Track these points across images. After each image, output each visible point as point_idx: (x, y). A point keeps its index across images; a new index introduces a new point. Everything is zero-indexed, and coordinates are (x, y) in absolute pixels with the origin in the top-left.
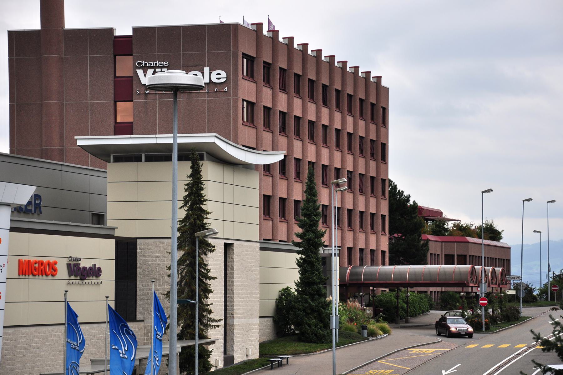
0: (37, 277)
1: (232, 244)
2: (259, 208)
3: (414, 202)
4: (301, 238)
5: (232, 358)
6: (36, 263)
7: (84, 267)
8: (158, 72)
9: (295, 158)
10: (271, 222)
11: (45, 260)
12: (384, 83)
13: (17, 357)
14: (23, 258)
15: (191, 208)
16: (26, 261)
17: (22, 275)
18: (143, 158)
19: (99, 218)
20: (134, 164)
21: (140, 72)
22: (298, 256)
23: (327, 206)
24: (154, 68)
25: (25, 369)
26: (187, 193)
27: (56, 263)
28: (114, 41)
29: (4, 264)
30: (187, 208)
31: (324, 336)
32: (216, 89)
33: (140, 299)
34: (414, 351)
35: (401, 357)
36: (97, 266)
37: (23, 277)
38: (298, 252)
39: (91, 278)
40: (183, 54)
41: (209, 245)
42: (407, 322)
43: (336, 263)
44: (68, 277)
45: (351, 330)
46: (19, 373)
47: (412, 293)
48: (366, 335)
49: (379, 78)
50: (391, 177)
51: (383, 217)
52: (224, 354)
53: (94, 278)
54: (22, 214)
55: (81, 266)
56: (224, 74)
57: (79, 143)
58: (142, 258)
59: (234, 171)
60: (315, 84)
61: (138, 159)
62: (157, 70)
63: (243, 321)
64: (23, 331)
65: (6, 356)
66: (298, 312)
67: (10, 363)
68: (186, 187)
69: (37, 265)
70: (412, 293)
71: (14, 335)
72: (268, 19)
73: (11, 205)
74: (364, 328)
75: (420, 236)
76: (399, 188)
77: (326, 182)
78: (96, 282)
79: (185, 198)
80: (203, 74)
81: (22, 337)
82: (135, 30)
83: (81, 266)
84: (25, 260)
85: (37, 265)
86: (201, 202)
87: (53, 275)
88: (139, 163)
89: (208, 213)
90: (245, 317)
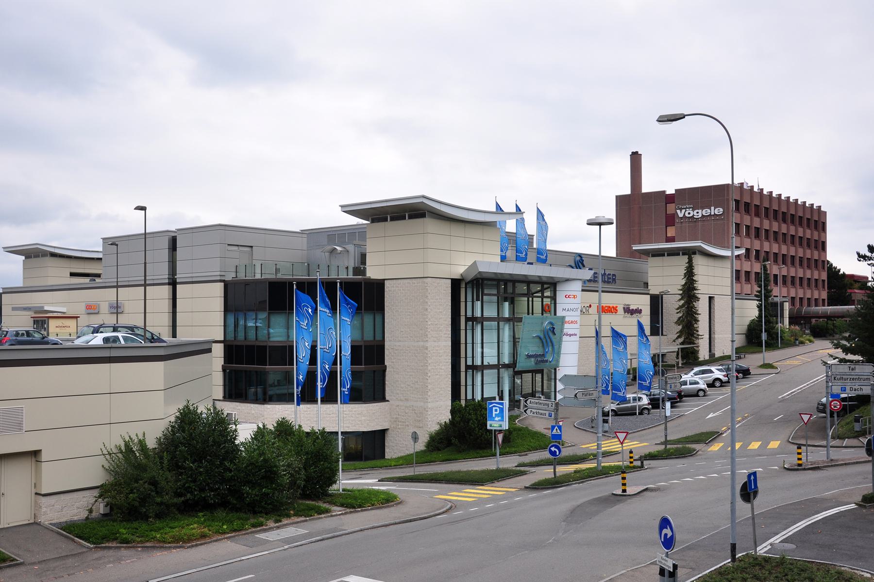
0: (607, 314)
1: (714, 297)
2: (119, 289)
3: (844, 272)
4: (759, 293)
5: (714, 354)
6: (606, 307)
7: (632, 309)
8: (25, 309)
9: (765, 251)
10: (750, 285)
11: (611, 305)
12: (822, 209)
15: (688, 278)
18: (666, 255)
19: (646, 285)
20: (661, 258)
21: (678, 211)
22: (757, 302)
23: (786, 276)
24: (686, 208)
26: (686, 271)
27: (617, 307)
28: (666, 197)
30: (685, 279)
31: (772, 344)
32: (718, 218)
33: (665, 325)
34: (821, 351)
35: (814, 354)
36: (639, 308)
38: (758, 300)
39: (637, 314)
40: (701, 201)
41: (697, 298)
42: (833, 337)
43: (787, 306)
45: (790, 341)
47: (838, 322)
48: (797, 343)
49: (820, 207)
50: (828, 259)
51: (823, 281)
52: (709, 352)
53: (638, 314)
54: (606, 284)
55: (631, 308)
56: (721, 210)
57: (634, 248)
58: (666, 304)
60: (778, 212)
61: (663, 255)
62: (687, 210)
63: (721, 336)
66: (757, 331)
68: (685, 268)
69: (607, 308)
70: (838, 322)
72: (682, 117)
74: (797, 340)
75: (846, 290)
76: (834, 265)
77: (786, 262)
78: (639, 316)
79: (685, 274)
80: (711, 210)
82: (676, 190)
83: (631, 308)
85: (607, 308)
86: (693, 276)
87: (616, 313)
88: (386, 223)
89: (697, 281)
90: (722, 334)
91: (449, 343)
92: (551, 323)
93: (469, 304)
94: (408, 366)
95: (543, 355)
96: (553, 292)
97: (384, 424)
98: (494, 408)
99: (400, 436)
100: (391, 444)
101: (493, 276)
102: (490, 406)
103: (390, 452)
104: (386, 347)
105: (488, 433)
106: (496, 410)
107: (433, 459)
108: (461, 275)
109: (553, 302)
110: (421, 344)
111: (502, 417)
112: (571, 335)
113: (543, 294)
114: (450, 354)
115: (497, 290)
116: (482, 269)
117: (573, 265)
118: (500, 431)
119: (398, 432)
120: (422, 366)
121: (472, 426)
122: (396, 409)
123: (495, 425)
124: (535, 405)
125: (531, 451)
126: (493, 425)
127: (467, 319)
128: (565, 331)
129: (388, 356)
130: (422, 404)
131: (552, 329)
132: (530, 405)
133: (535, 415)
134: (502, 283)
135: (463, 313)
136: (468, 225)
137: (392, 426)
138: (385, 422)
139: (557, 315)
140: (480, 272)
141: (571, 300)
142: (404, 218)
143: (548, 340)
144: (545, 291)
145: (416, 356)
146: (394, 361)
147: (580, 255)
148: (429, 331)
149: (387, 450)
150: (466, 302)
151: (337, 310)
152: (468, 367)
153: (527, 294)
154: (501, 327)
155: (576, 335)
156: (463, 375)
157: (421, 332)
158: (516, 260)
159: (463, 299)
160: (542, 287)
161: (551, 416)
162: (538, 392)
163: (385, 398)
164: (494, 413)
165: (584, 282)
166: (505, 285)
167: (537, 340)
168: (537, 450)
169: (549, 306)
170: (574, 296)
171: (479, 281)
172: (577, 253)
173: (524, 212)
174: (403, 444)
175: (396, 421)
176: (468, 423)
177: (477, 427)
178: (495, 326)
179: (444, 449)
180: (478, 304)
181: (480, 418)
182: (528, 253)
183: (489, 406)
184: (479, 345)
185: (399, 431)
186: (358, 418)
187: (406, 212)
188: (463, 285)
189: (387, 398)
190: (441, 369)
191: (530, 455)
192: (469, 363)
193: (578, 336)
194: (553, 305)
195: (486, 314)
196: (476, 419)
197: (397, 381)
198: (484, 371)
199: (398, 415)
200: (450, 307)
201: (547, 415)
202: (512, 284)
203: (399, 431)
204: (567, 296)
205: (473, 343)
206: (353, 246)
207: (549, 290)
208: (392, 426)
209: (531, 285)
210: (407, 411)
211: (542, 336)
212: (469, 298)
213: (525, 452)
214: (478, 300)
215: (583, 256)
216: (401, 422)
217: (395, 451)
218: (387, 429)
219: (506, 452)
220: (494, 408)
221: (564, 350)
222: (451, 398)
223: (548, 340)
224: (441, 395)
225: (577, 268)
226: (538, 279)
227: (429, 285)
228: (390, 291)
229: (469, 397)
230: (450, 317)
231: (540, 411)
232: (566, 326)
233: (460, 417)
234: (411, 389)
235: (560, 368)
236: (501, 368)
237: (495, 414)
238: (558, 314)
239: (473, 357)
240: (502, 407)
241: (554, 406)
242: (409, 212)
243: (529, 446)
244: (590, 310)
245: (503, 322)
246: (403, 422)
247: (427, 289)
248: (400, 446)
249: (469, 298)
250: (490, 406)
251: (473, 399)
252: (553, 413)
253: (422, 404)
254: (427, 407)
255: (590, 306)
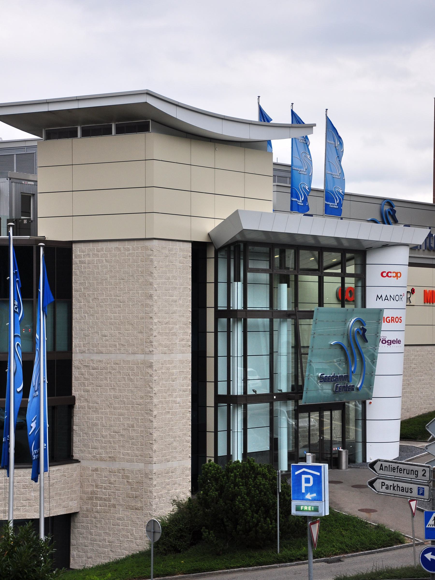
13: (424, 370)
14: (428, 289)
16: (431, 291)
17: (427, 303)
25: (432, 380)
29: (404, 294)
37: (428, 304)
44: (423, 304)
46: (426, 383)
54: (432, 252)
59: (215, 149)
64: (429, 349)
65: (415, 369)
67: (419, 375)
71: (421, 352)
73: (409, 245)
81: (428, 354)
84: (429, 291)
85: (390, 319)
88: (75, 140)
91: (189, 356)
92: (359, 321)
93: (222, 288)
94: (115, 397)
95: (347, 378)
96: (359, 267)
97: (71, 503)
98: (304, 477)
99: (99, 525)
100: (81, 541)
101: (262, 238)
102: (297, 473)
103: (79, 556)
104: (76, 362)
105: (268, 519)
106: (307, 481)
107: (169, 570)
108: (209, 234)
109: (360, 284)
110: (140, 357)
111: (319, 493)
112: (390, 342)
113: (343, 269)
114: (190, 376)
115: (268, 263)
116: (247, 225)
117: (378, 219)
118: (314, 520)
119: (95, 518)
120: (142, 398)
121: (241, 505)
122: (92, 475)
123: (306, 508)
124: (392, 473)
125: (347, 553)
126: (302, 508)
127: (219, 314)
128: (383, 335)
129: (77, 379)
130: (141, 466)
131: (361, 332)
132: (381, 472)
133: (391, 491)
134: (277, 250)
135: (210, 302)
136: (218, 146)
137: (85, 508)
138: (72, 500)
139: (368, 307)
140: (243, 232)
141: (392, 281)
142: (107, 132)
143: (355, 351)
144: (347, 263)
145: (131, 380)
146: (89, 388)
147: (390, 202)
148: (154, 334)
149: (74, 552)
150: (216, 283)
151: (8, 296)
152: (219, 399)
153: (318, 270)
154: (275, 328)
155: (399, 342)
156: (210, 412)
157: (140, 336)
158: (292, 209)
159: (210, 277)
160: (343, 256)
161: (423, 494)
162: (337, 443)
163: (73, 456)
164: (304, 485)
165: (414, 248)
166: (282, 253)
167: (338, 351)
168: (357, 551)
169: (351, 291)
170: (397, 273)
171: (239, 246)
172: (384, 199)
173: (315, 125)
174: (105, 540)
175: (91, 499)
176: (233, 500)
177: (250, 508)
178: (264, 326)
179: (186, 549)
180: (238, 287)
181: (255, 490)
182: (309, 198)
183: (294, 473)
184: (240, 361)
185: (98, 515)
186: (23, 494)
187: (111, 120)
188: (211, 253)
189: (76, 456)
190: (175, 402)
191: (346, 560)
192: (222, 390)
193: (403, 343)
194: (359, 290)
195: (251, 305)
196: (248, 494)
197: (95, 425)
198: (249, 406)
199: (97, 486)
200: (191, 293)
201: (415, 491)
202: (293, 251)
203: (98, 515)
204: (385, 274)
205: (229, 356)
206: (8, 182)
207: (353, 262)
208: (85, 508)
209: (325, 254)
210: (112, 479)
211: (345, 343)
212: (222, 276)
213: (336, 554)
214: (237, 279)
215: (395, 204)
216: (101, 499)
217: (89, 555)
218: (75, 514)
219: (301, 555)
220: (304, 477)
221: (380, 369)
222: (190, 455)
223: (355, 351)
224: (175, 449)
225: (384, 223)
226: (334, 243)
227: (155, 253)
228: (81, 262)
229: (222, 452)
230: (190, 310)
231: (401, 484)
232: (385, 326)
233: (217, 490)
234: (122, 439)
235: (373, 401)
236: (277, 400)
237: (306, 487)
238: (369, 306)
239: (229, 381)
240: (318, 474)
241: (427, 474)
242: (118, 121)
243: (341, 543)
244: (413, 298)
245: (278, 319)
246: (105, 500)
247: (152, 261)
248: (99, 545)
249: (222, 276)
250: (297, 473)
251: (229, 456)
252: (426, 488)
253: (141, 466)
254: (151, 471)
255: (413, 291)
